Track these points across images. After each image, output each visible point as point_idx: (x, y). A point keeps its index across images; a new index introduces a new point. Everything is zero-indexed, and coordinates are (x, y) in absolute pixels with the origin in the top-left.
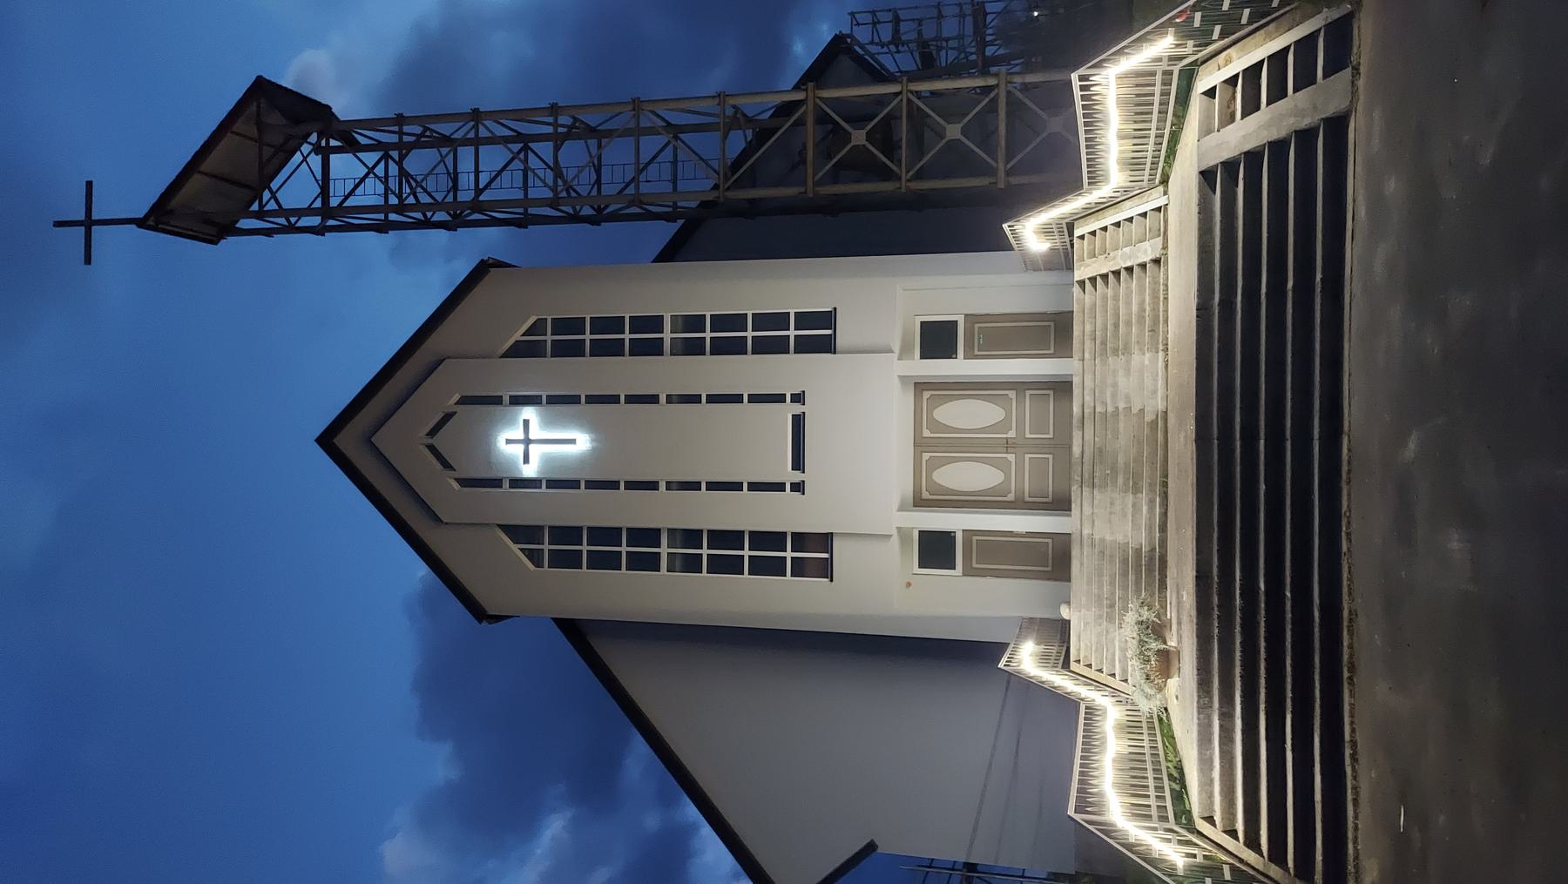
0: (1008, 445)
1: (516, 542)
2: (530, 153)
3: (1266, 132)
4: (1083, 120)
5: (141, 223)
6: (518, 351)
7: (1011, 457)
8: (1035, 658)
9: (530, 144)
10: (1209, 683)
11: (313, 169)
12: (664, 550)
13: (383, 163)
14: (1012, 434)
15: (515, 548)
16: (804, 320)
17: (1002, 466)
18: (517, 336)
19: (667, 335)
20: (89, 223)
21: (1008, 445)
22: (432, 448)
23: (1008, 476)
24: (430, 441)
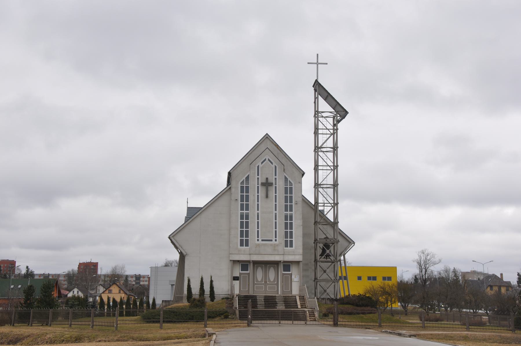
0: (266, 282)
1: (246, 178)
2: (331, 171)
3: (329, 292)
4: (275, 194)
5: (316, 81)
6: (286, 179)
7: (263, 283)
8: (112, 269)
9: (333, 171)
10: (475, 272)
11: (330, 277)
12: (245, 212)
13: (331, 133)
14: (268, 283)
15: (244, 178)
16: (291, 242)
17: (262, 280)
18: (289, 179)
19: (289, 213)
20: (317, 64)
21: (266, 282)
22: (265, 160)
23: (260, 282)
24: (267, 159)
